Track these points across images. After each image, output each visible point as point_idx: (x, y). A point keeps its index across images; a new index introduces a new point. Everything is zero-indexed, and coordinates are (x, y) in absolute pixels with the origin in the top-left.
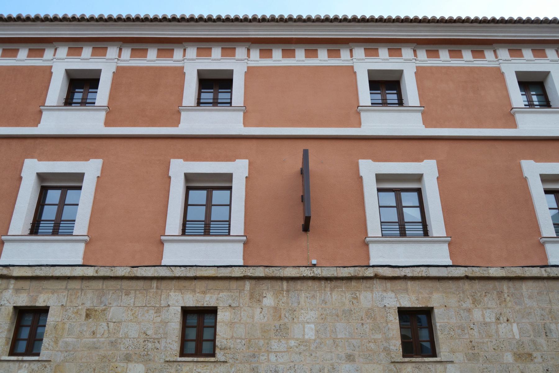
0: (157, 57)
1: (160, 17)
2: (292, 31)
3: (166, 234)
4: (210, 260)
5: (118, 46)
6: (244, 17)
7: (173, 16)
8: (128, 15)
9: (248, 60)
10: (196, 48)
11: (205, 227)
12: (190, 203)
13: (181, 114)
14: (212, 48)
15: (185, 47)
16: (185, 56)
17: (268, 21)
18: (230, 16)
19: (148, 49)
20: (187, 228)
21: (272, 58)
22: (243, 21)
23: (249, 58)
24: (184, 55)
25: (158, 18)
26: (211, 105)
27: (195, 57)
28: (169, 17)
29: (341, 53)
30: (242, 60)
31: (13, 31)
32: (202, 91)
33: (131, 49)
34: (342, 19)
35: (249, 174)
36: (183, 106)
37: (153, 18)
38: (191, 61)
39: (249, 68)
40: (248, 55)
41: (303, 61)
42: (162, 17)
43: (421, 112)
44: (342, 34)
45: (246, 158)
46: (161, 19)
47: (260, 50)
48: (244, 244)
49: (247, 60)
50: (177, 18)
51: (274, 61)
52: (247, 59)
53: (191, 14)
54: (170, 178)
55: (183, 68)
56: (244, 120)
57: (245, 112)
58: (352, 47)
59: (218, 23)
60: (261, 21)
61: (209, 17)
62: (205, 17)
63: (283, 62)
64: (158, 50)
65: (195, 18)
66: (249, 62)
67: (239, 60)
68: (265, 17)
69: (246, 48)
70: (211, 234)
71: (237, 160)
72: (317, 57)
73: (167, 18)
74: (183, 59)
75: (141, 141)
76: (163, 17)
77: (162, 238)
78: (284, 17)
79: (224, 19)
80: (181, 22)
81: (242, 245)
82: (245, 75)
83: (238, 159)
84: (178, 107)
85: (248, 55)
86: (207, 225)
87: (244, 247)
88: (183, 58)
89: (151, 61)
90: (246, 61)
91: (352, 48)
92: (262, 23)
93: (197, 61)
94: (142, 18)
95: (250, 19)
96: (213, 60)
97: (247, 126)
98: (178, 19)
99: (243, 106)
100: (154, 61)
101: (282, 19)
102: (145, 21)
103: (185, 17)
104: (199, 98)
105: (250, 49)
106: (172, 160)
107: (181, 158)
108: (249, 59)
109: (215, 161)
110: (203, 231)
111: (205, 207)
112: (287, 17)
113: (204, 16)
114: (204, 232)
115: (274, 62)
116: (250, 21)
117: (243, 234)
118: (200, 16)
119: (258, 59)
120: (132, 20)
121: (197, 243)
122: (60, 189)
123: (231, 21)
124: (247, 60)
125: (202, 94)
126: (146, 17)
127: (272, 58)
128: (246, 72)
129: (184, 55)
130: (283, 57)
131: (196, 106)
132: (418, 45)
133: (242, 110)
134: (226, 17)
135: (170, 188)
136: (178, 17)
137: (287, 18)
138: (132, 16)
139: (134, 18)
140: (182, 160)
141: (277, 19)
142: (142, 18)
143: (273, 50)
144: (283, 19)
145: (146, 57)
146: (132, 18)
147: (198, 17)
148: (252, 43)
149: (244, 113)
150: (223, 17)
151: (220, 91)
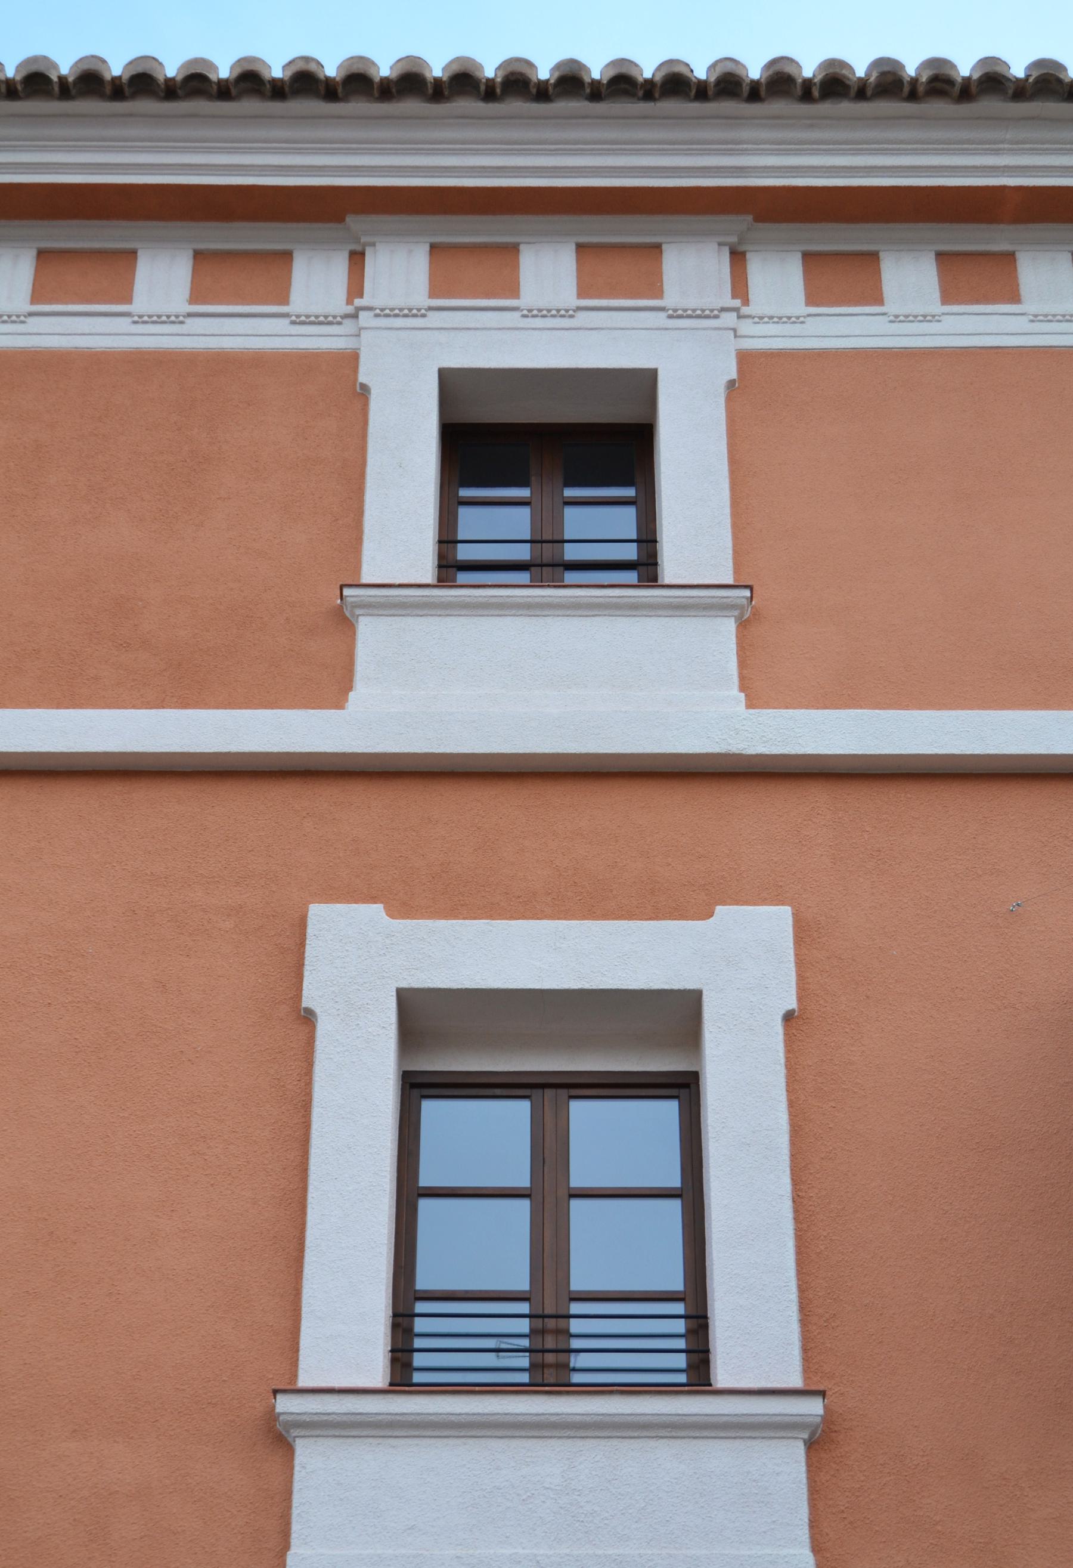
0: (194, 299)
1: (224, 73)
2: (997, 152)
3: (303, 1382)
4: (600, 1552)
5: (722, 239)
6: (294, 69)
7: (300, 66)
8: (34, 59)
9: (739, 317)
10: (427, 247)
11: (533, 1333)
12: (427, 1178)
13: (354, 633)
14: (522, 247)
15: (357, 240)
16: (361, 295)
17: (862, 92)
18: (636, 65)
19: (139, 253)
20: (418, 1343)
21: (879, 300)
22: (710, 93)
23: (746, 302)
24: (356, 288)
25: (213, 77)
26: (524, 577)
27: (420, 297)
28: (277, 73)
29: (1019, 269)
30: (708, 317)
31: (396, 152)
32: (465, 493)
33: (33, 253)
34: (552, 81)
35: (802, 994)
36: (364, 581)
37: (179, 78)
38: (399, 322)
39: (745, 359)
40: (740, 287)
41: (798, 320)
42: (235, 74)
43: (736, 613)
44: (966, 167)
45: (777, 900)
46: (227, 80)
47: (580, 248)
48: (811, 1446)
49: (735, 314)
50: (322, 77)
51: (896, 319)
52: (736, 310)
53: (404, 55)
54: (308, 1019)
55: (352, 359)
56: (742, 664)
57: (748, 620)
58: (363, 240)
59: (561, 106)
60: (816, 93)
61: (512, 73)
62: (489, 72)
63: (950, 324)
64: (199, 256)
65: (428, 75)
66: (746, 327)
67: (689, 317)
68: (845, 72)
69: (720, 244)
70: (577, 1378)
71: (719, 909)
72: (1014, 296)
73: (266, 75)
74: (350, 309)
75: (114, 792)
76: (238, 71)
77: (285, 1405)
78: (952, 73)
79: (599, 82)
80: (345, 99)
81: (798, 1450)
82: (729, 399)
83: (724, 903)
84: (342, 587)
85: (740, 287)
86: (551, 1323)
87: (809, 1465)
88: (349, 302)
89: (158, 319)
90: (729, 319)
91: (365, 245)
92: (826, 108)
93: (435, 319)
94: (120, 78)
95: (755, 85)
96: (530, 313)
97: (767, 705)
98: (328, 80)
99: (730, 581)
100: (176, 319)
101: (938, 85)
102: (134, 96)
103: (372, 72)
104: (447, 540)
105: (743, 254)
106: (316, 910)
107: (373, 899)
108: (745, 310)
109: (584, 918)
110: (524, 1361)
111: (525, 1204)
112: (973, 69)
113: (480, 67)
114: (533, 1368)
115: (896, 328)
116: (755, 93)
117: (796, 1381)
118: (456, 68)
119: (800, 307)
120: (56, 88)
121: (506, 1441)
122: (673, 1092)
123: (641, 93)
124: (735, 314)
125: (465, 514)
126: (140, 69)
127: (879, 300)
128: (731, 384)
129: (356, 288)
130: (947, 297)
131: (435, 582)
132: (760, 225)
133: (732, 607)
134: (611, 73)
135: (309, 1084)
136: (331, 70)
137: (976, 76)
138: (55, 66)
139: (71, 79)
140: (377, 910)
141: (914, 81)
142: (115, 80)
143: (882, 255)
144: (949, 81)
145: (128, 299)
146: (55, 79)
147: (444, 69)
148: (760, 218)
149: (743, 625)
150: (596, 70)
151: (569, 493)
